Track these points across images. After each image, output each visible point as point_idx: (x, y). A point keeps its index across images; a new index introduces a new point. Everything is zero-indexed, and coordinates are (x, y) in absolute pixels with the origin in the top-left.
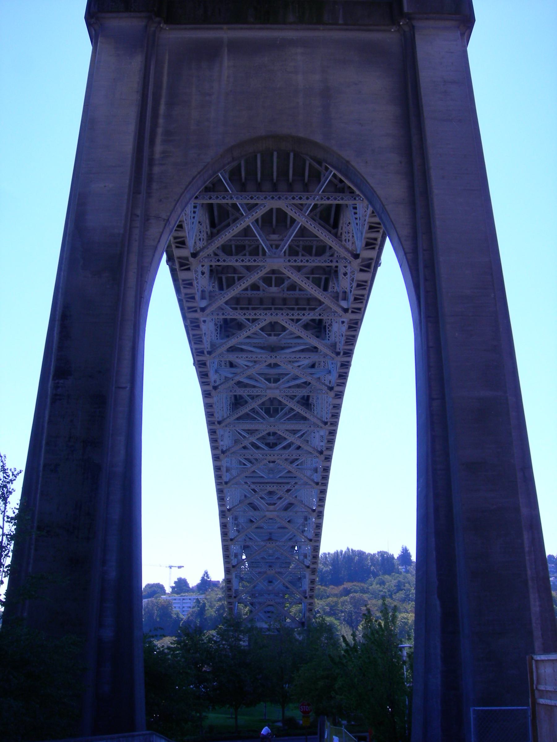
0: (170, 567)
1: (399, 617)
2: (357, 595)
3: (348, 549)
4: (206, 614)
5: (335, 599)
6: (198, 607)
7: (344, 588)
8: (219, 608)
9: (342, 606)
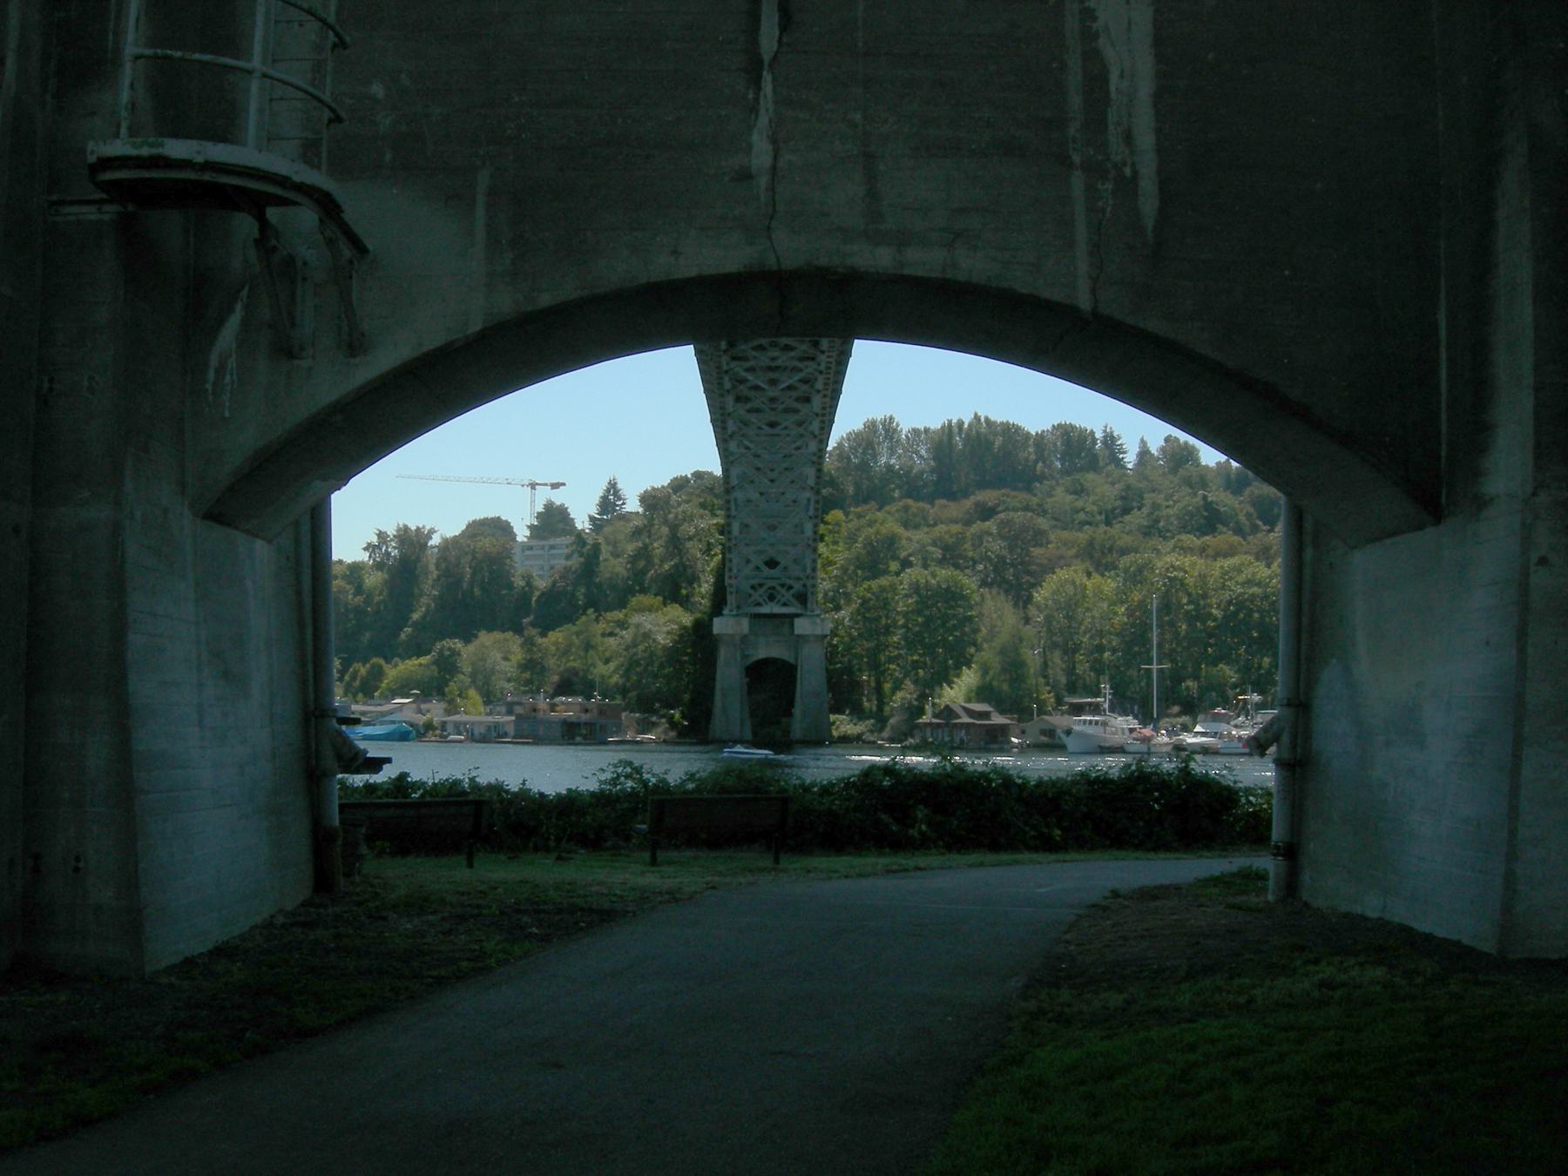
0: (533, 486)
1: (1159, 564)
2: (1019, 517)
3: (977, 417)
4: (600, 572)
5: (955, 528)
6: (581, 555)
7: (977, 504)
8: (635, 556)
9: (975, 547)
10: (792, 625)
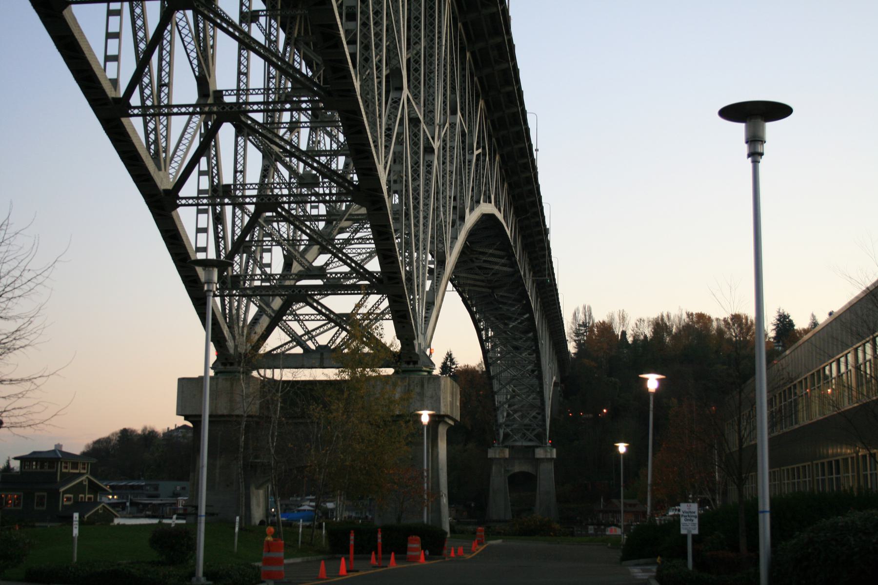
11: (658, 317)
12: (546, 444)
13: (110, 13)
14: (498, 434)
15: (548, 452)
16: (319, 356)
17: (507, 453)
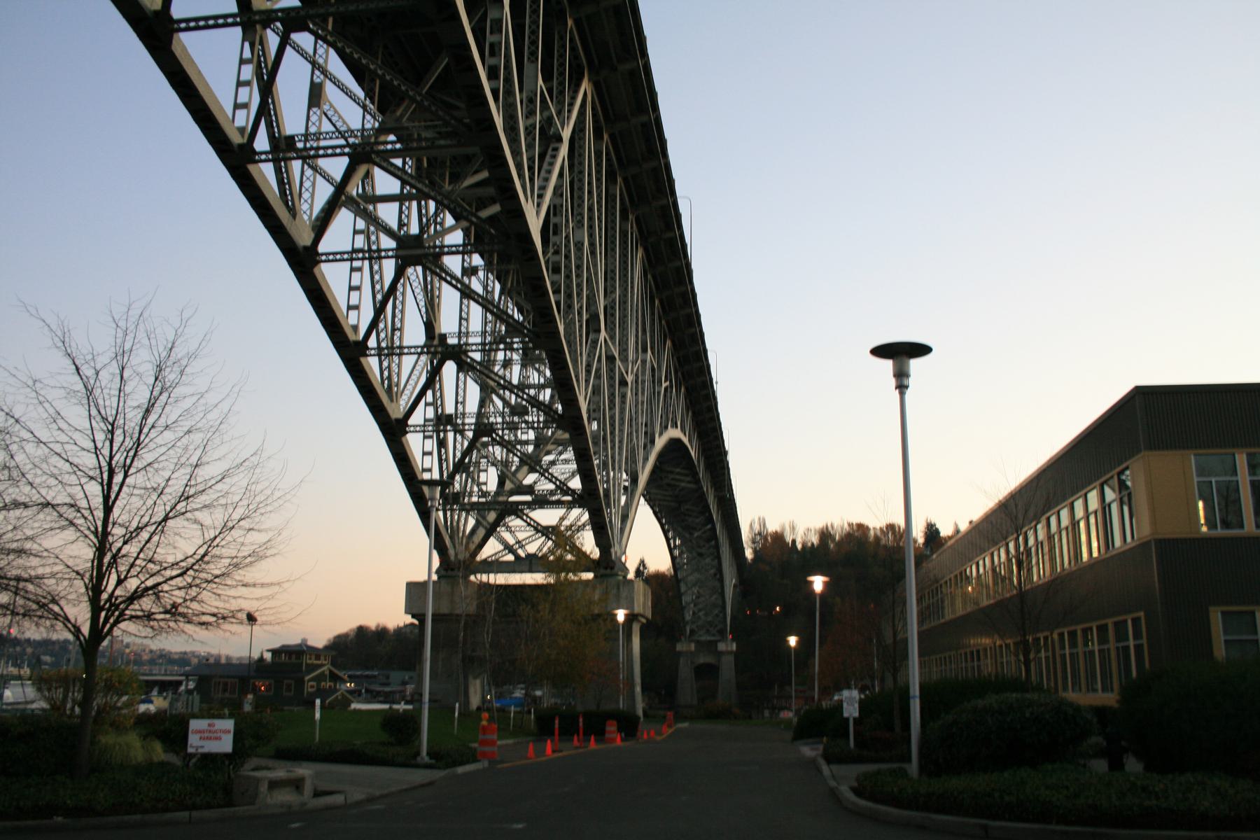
10: (716, 647)
11: (823, 528)
12: (727, 638)
13: (353, 270)
14: (685, 630)
15: (728, 646)
16: (528, 562)
17: (693, 647)
